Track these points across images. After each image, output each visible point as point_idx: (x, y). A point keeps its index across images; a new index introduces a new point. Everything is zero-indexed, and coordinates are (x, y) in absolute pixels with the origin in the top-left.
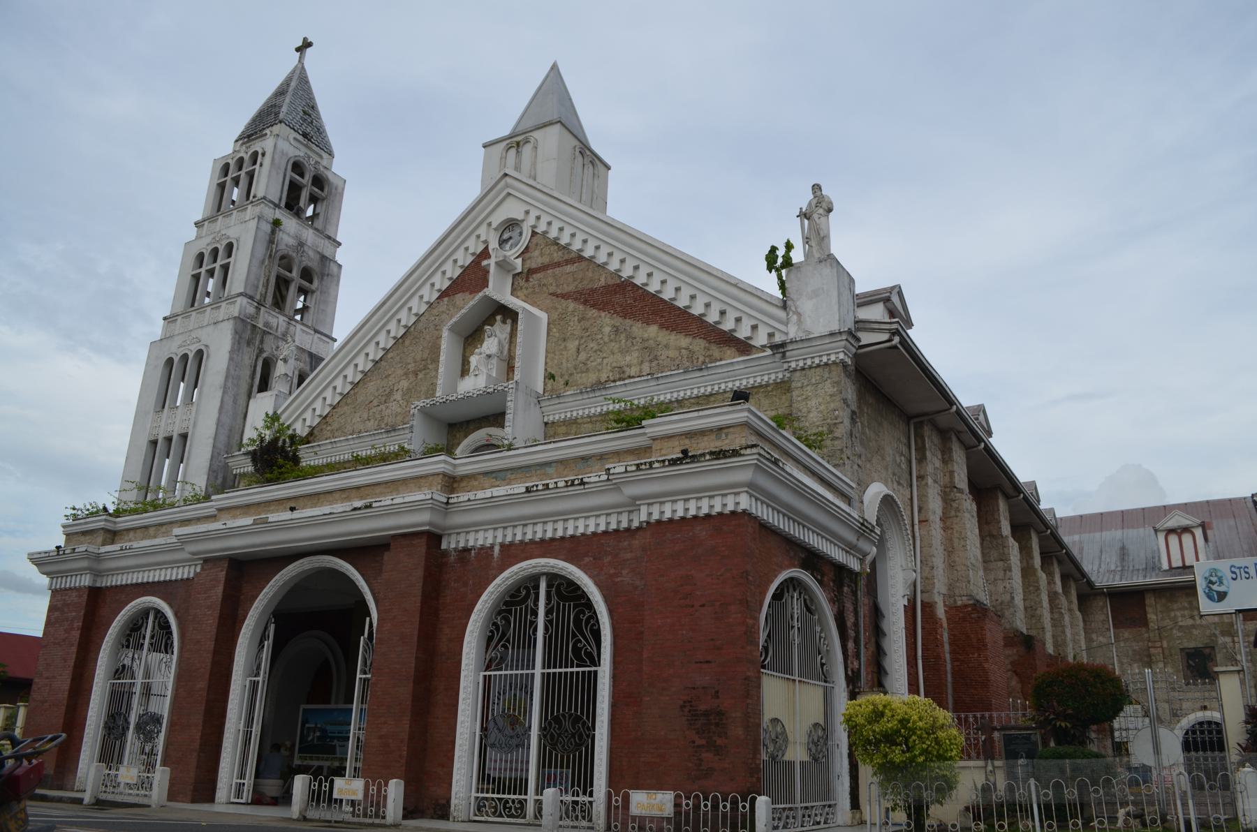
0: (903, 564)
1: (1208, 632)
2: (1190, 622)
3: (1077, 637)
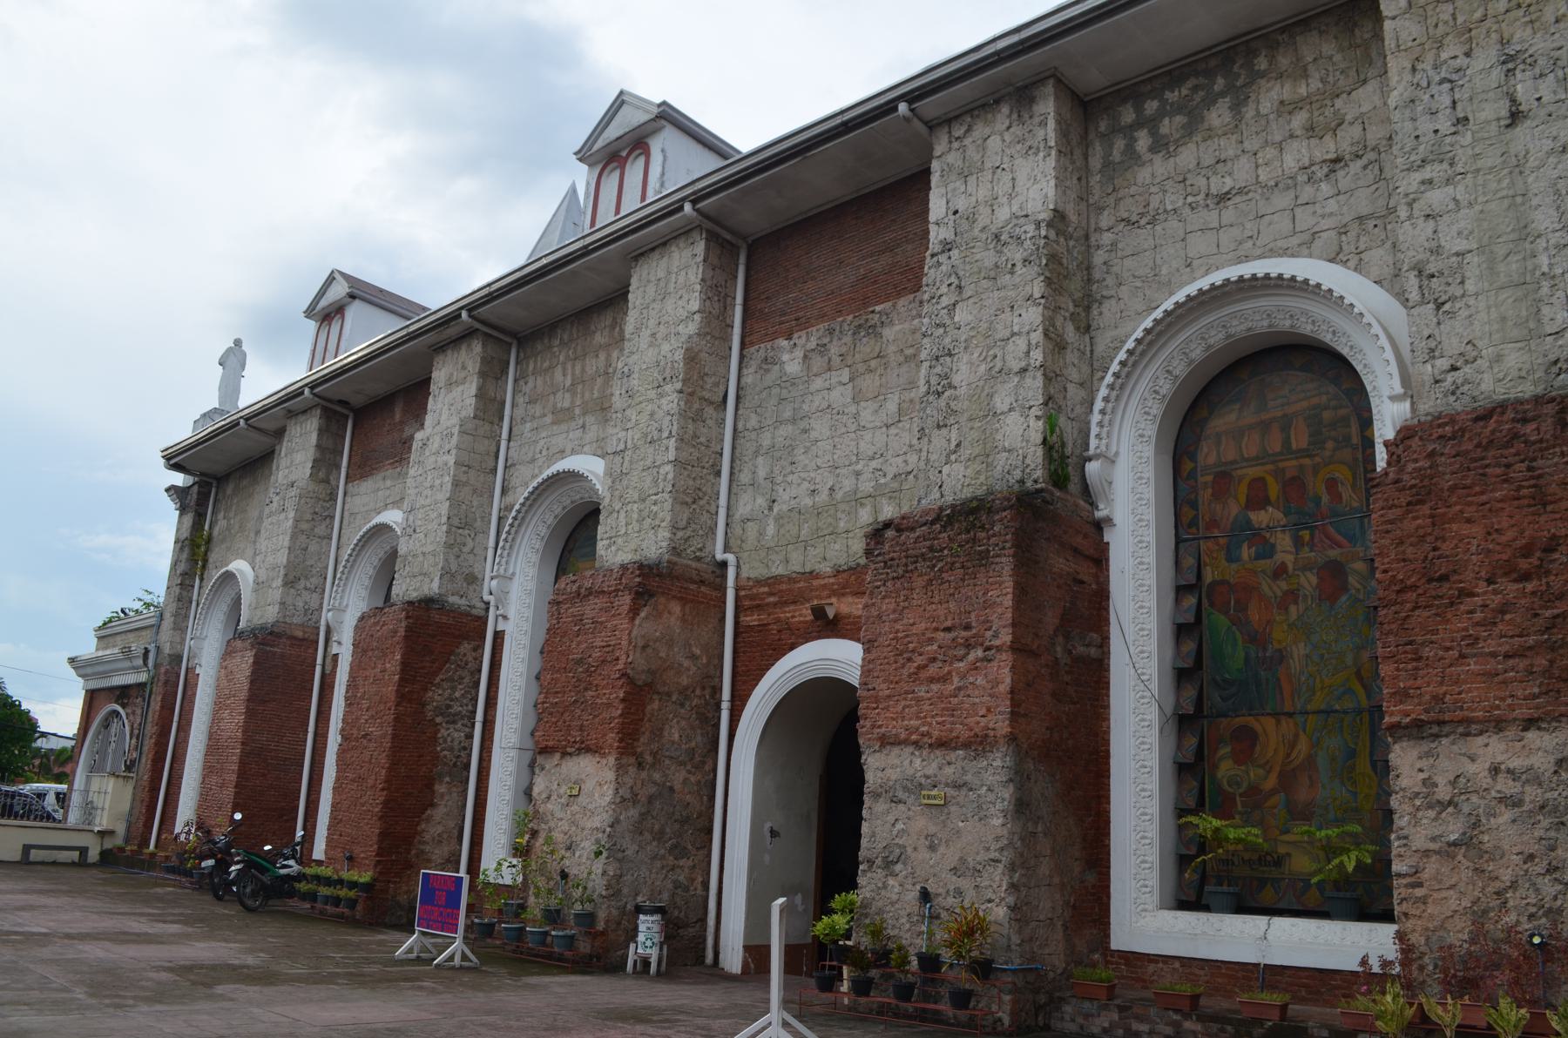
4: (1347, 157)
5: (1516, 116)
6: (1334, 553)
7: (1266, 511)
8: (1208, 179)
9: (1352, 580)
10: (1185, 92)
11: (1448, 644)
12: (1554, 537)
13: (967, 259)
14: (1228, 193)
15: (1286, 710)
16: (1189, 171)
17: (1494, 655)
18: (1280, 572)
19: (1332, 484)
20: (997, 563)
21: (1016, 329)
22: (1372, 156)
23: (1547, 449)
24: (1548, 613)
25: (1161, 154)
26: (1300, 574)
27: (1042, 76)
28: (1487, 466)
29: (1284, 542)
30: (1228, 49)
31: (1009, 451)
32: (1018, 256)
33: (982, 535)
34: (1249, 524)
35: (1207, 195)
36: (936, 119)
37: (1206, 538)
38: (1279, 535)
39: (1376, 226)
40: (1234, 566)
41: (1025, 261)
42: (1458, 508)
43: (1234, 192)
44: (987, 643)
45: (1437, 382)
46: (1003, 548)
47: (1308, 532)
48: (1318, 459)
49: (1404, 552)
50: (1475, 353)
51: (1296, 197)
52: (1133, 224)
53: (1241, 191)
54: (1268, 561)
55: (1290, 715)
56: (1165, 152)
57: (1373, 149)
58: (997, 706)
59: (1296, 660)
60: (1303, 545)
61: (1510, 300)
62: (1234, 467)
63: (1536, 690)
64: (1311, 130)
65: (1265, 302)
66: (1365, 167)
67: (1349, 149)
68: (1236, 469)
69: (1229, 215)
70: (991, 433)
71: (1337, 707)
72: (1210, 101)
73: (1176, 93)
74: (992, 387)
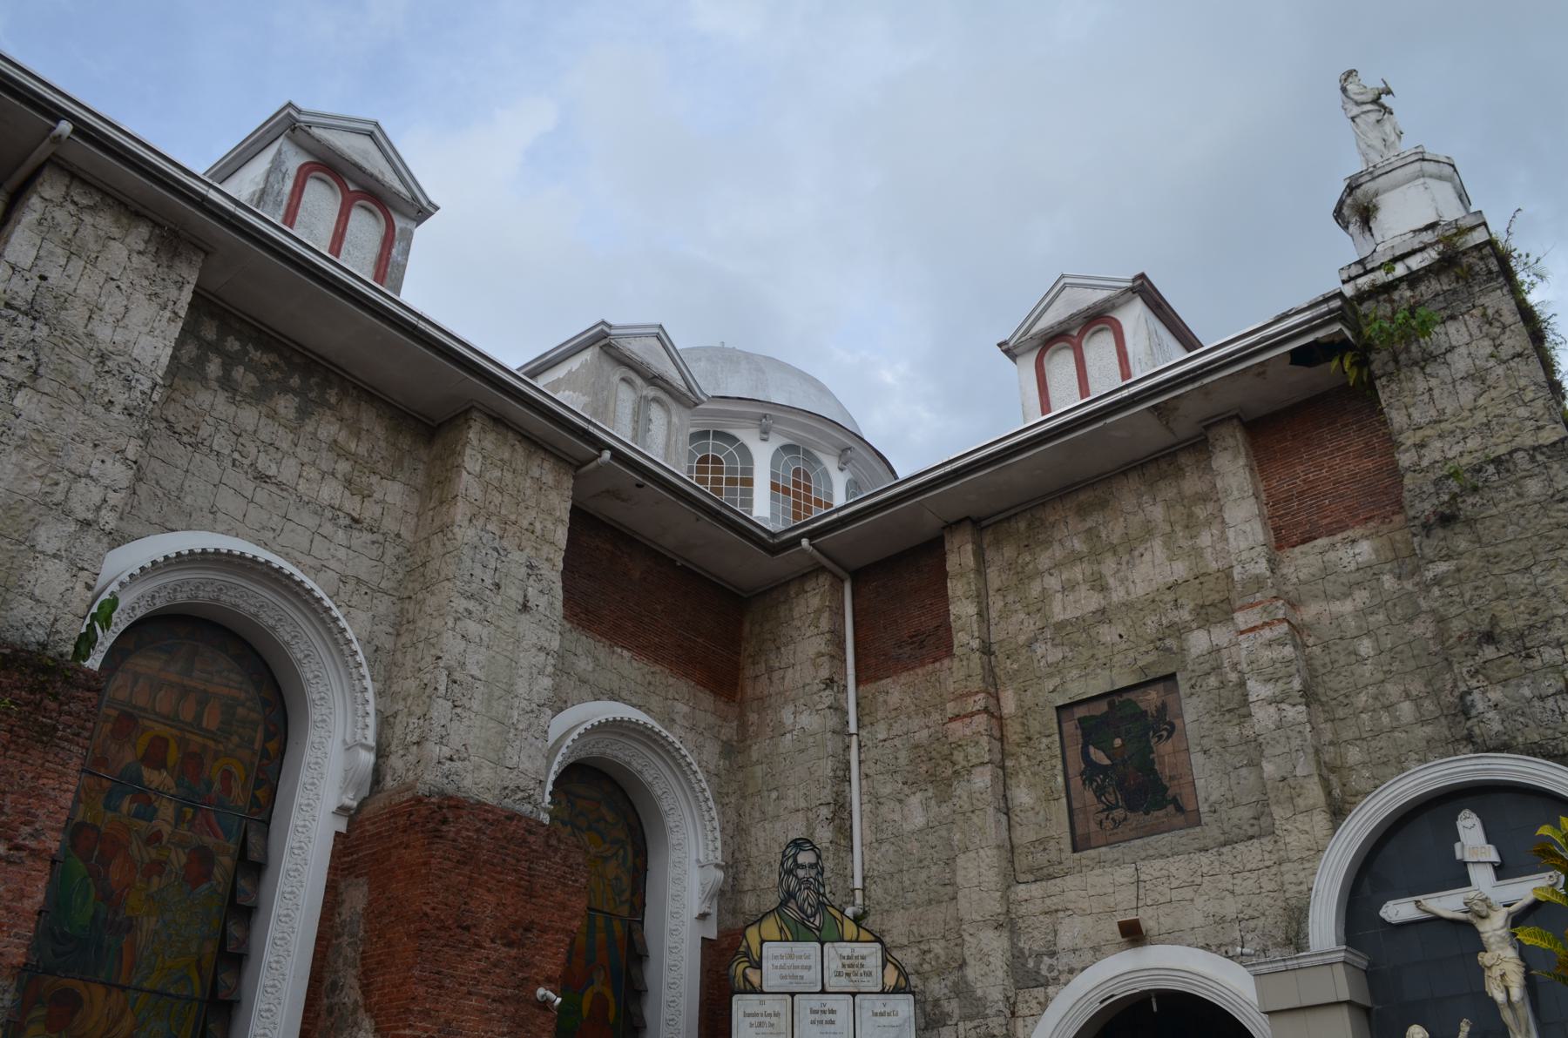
0: (701, 859)
1: (1151, 625)
2: (1091, 601)
3: (840, 773)
4: (365, 525)
5: (525, 608)
6: (208, 840)
7: (160, 774)
8: (259, 451)
9: (217, 871)
10: (265, 360)
11: (462, 981)
12: (532, 922)
13: (57, 349)
14: (269, 477)
15: (120, 982)
16: (246, 431)
17: (487, 996)
18: (155, 838)
19: (227, 776)
20: (63, 748)
21: (94, 472)
22: (380, 538)
23: (540, 859)
24: (520, 975)
25: (226, 394)
26: (173, 847)
27: (146, 212)
28: (508, 855)
29: (167, 810)
30: (313, 361)
31: (38, 601)
32: (121, 398)
33: (53, 705)
34: (138, 779)
35: (252, 465)
36: (67, 162)
37: (90, 773)
38: (165, 802)
39: (366, 593)
40: (109, 815)
41: (125, 409)
42: (485, 877)
43: (273, 480)
44: (20, 841)
45: (439, 762)
46: (78, 735)
47: (192, 810)
48: (221, 747)
49: (447, 897)
50: (466, 755)
51: (320, 525)
52: (175, 433)
53: (278, 484)
54: (144, 823)
55: (124, 988)
56: (230, 395)
57: (383, 534)
58: (14, 926)
59: (144, 934)
60: (184, 821)
61: (494, 730)
62: (142, 714)
63: (505, 1030)
64: (348, 483)
65: (266, 594)
66: (373, 543)
67: (368, 520)
68: (144, 717)
69: (261, 496)
70: (20, 567)
71: (172, 991)
72: (285, 390)
73: (259, 354)
74: (41, 515)
